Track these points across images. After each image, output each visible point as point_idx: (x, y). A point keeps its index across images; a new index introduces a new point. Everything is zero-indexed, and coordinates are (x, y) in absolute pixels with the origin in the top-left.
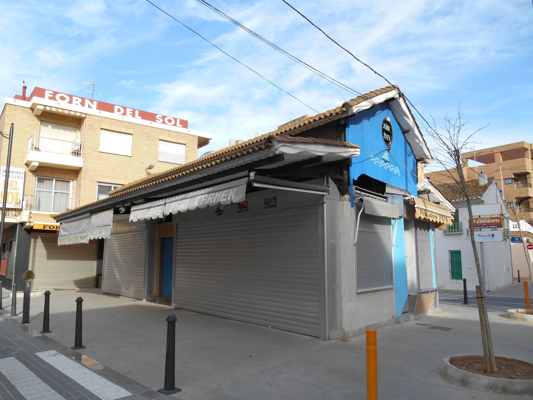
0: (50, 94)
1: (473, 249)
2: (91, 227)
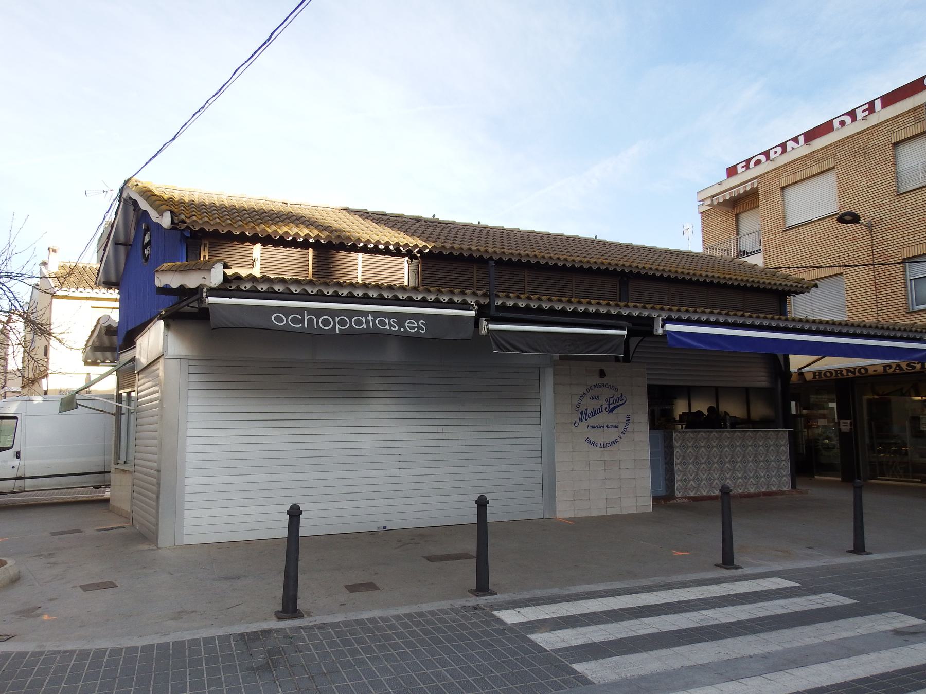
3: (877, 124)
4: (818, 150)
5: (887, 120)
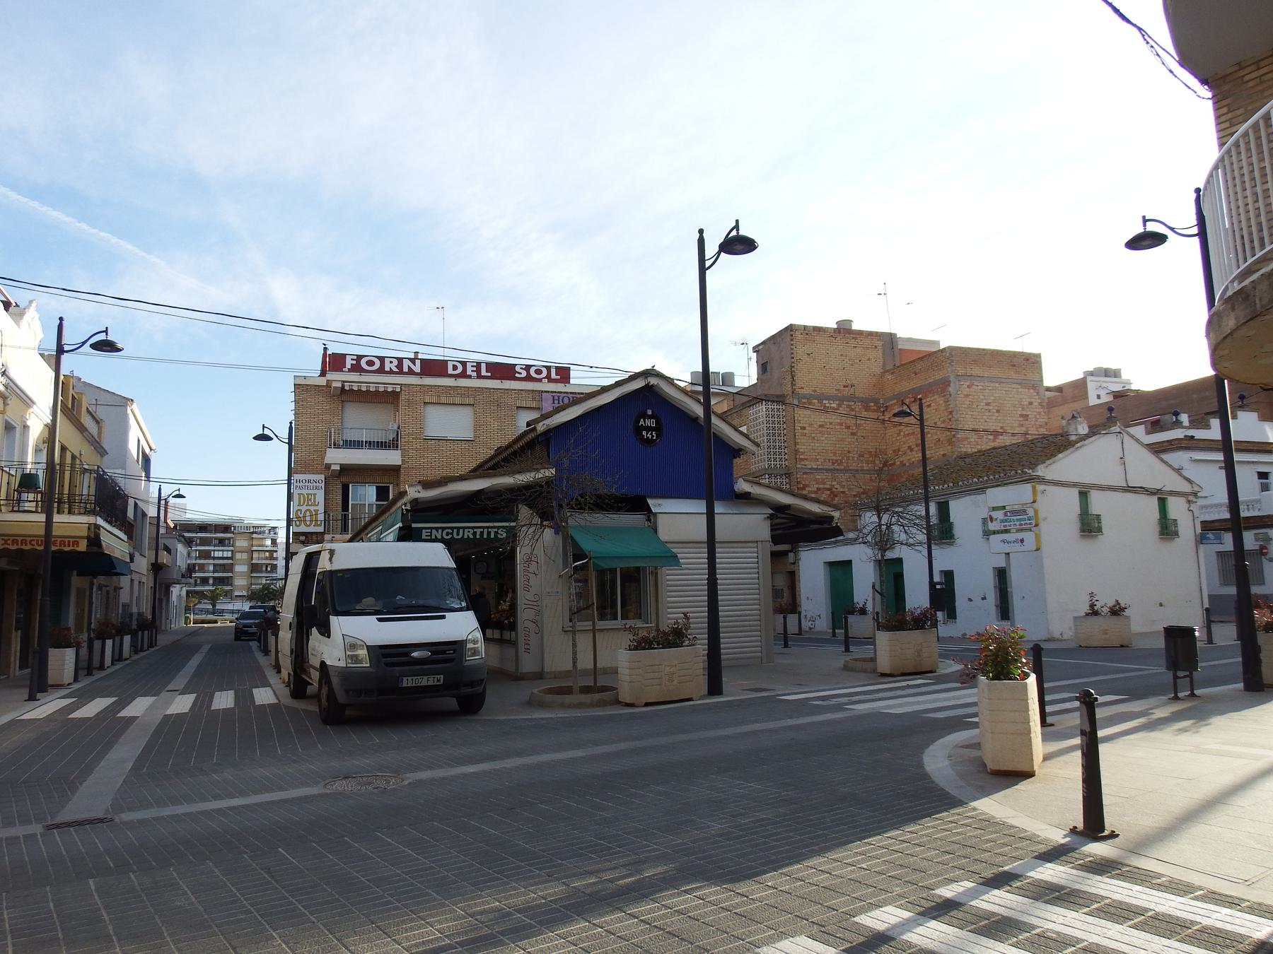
0: (352, 359)
2: (636, 575)
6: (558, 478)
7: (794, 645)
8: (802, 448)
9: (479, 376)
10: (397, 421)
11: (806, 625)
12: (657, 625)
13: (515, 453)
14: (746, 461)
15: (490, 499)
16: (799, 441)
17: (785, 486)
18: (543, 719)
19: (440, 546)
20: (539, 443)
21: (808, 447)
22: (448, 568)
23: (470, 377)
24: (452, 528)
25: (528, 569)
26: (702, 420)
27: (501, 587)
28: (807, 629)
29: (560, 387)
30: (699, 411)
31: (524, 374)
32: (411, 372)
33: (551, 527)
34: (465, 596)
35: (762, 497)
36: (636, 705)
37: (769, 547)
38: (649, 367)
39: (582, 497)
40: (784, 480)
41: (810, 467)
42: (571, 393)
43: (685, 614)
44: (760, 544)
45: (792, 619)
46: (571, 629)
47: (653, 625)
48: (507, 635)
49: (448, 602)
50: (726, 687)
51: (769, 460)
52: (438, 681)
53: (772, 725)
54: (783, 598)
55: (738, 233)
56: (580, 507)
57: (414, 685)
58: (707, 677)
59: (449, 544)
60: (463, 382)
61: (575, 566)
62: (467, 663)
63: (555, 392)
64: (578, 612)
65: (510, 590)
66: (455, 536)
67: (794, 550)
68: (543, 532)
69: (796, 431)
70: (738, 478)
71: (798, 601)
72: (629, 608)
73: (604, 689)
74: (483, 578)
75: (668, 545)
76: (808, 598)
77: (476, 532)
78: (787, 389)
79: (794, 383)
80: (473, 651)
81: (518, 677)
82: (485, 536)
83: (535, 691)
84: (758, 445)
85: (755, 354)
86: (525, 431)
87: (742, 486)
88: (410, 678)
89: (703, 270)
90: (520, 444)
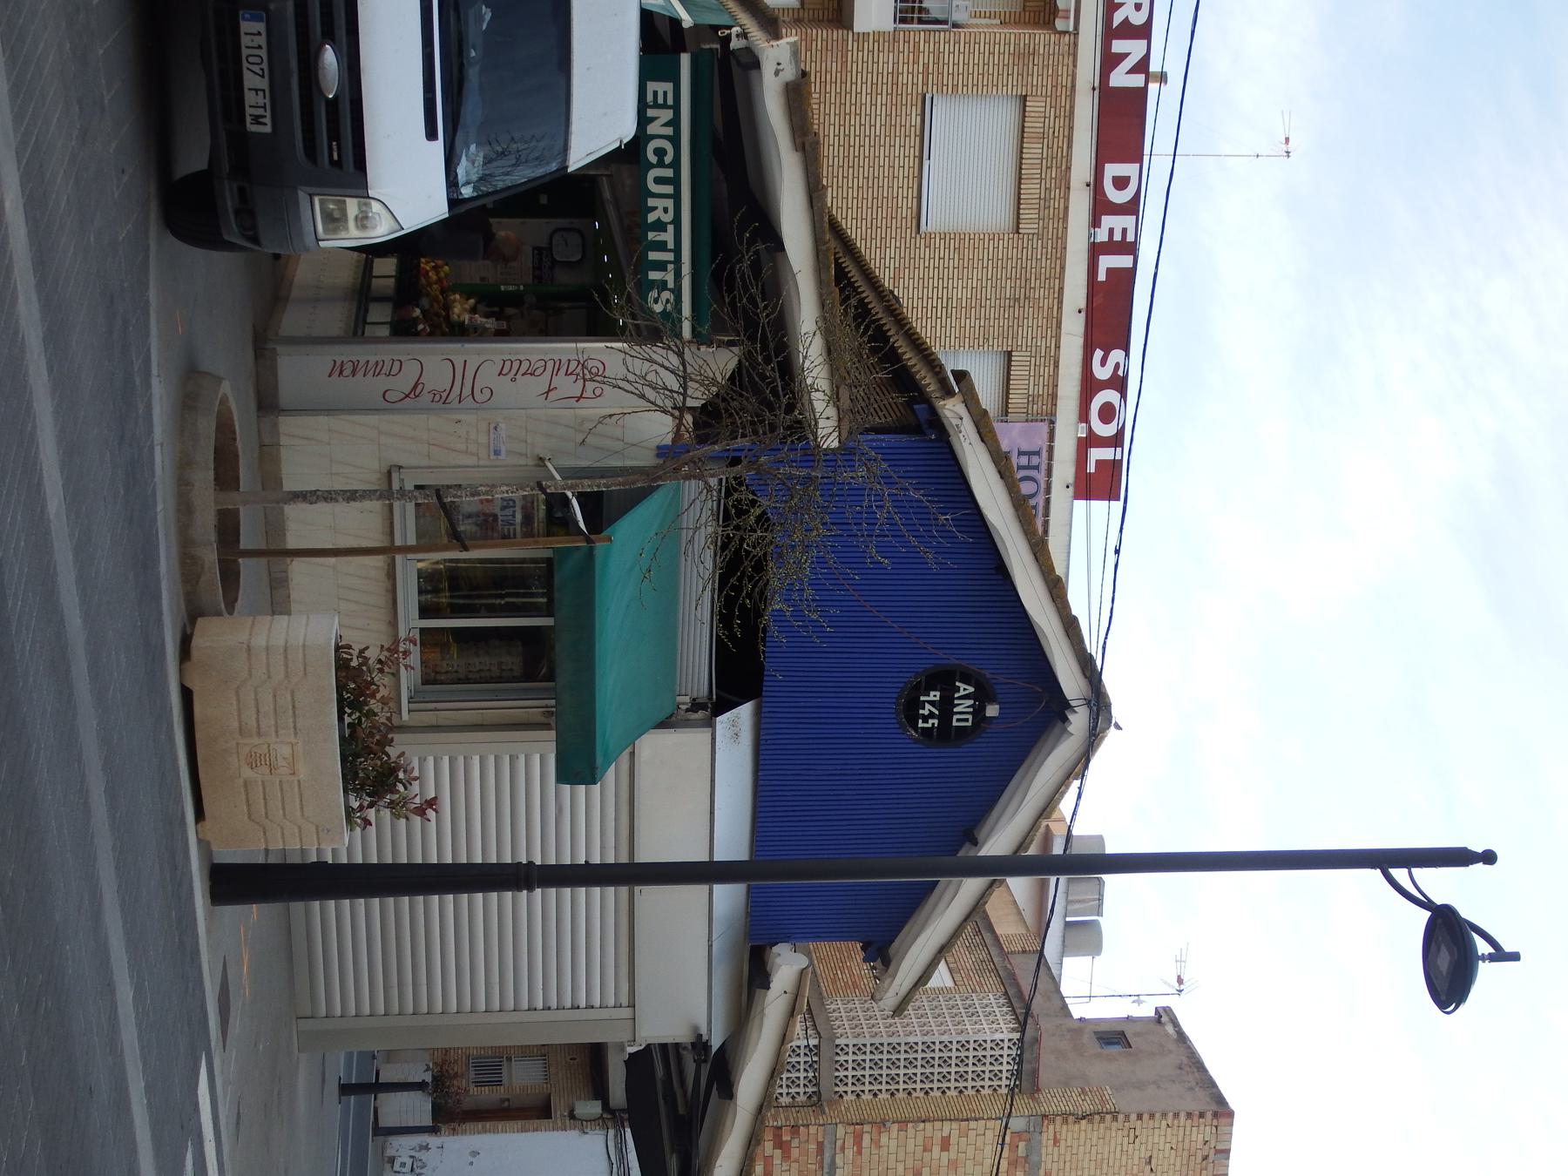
1: (15, 91)
3: (1060, 328)
4: (1067, 199)
5: (1059, 347)
6: (811, 453)
7: (345, 1113)
8: (891, 1139)
9: (1096, 250)
10: (974, 21)
11: (402, 1147)
12: (403, 729)
13: (880, 336)
14: (855, 985)
15: (756, 267)
16: (911, 1131)
17: (784, 1091)
18: (149, 407)
19: (627, 129)
20: (910, 403)
21: (892, 1157)
22: (565, 149)
23: (1095, 223)
24: (676, 165)
25: (563, 371)
26: (971, 854)
27: (515, 300)
28: (390, 1152)
29: (1064, 471)
30: (998, 842)
31: (1102, 373)
32: (1110, 62)
33: (677, 435)
34: (488, 194)
35: (757, 1021)
36: (187, 665)
37: (624, 1041)
38: (1117, 712)
39: (758, 519)
40: (801, 1090)
41: (839, 1161)
42: (1048, 501)
43: (432, 803)
44: (626, 1013)
45: (417, 1108)
46: (396, 486)
47: (405, 716)
48: (380, 313)
49: (473, 148)
50: (231, 913)
51: (859, 1049)
52: (257, 120)
53: (129, 1035)
54: (478, 1084)
55: (1483, 958)
56: (733, 512)
57: (245, 52)
58: (261, 860)
59: (630, 155)
60: (1080, 204)
61: (567, 501)
62: (302, 196)
63: (1050, 458)
64: (443, 506)
65: (504, 325)
66: (653, 173)
67: (611, 1118)
68: (665, 412)
69: (938, 1124)
70: (808, 954)
71: (467, 1126)
72: (454, 650)
73: (230, 577)
74: (538, 251)
75: (625, 757)
76: (475, 1154)
77: (665, 230)
78: (1051, 1101)
79: (1071, 1119)
80: (336, 215)
81: (263, 343)
82: (653, 256)
83: (226, 387)
84: (899, 1010)
85: (1152, 1013)
86: (941, 366)
87: (786, 965)
88: (262, 40)
89: (1382, 860)
90: (909, 357)
